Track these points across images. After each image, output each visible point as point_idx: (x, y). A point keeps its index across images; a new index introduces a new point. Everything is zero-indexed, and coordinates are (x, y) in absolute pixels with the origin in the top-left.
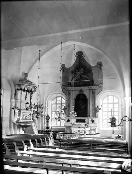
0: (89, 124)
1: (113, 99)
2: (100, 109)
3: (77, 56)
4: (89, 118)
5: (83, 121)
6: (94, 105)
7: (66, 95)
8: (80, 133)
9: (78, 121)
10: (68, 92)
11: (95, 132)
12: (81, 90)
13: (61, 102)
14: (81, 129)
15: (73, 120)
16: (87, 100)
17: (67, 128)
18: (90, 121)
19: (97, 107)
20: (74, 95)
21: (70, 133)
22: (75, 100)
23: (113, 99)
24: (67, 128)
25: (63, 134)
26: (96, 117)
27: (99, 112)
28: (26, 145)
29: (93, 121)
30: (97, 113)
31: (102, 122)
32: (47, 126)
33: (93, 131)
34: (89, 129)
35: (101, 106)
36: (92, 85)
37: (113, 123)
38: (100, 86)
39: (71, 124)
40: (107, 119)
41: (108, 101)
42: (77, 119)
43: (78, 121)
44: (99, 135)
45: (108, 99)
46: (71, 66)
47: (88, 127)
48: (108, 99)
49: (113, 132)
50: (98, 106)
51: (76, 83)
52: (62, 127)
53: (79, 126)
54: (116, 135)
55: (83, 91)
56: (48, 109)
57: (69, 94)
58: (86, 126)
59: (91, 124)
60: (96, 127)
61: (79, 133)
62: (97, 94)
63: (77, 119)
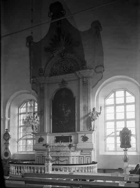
0: (78, 144)
1: (125, 97)
2: (100, 113)
3: (52, 14)
4: (77, 134)
5: (67, 139)
6: (86, 108)
7: (37, 92)
8: (60, 163)
9: (58, 140)
10: (41, 88)
11: (89, 160)
12: (63, 82)
13: (115, 116)
14: (61, 154)
15: (49, 139)
16: (75, 98)
17: (39, 153)
18: (80, 139)
19: (92, 110)
20: (51, 91)
21: (86, 163)
22: (53, 101)
23: (125, 97)
24: (39, 153)
25: (32, 166)
26: (90, 130)
27: (96, 121)
28: (52, 187)
29: (85, 139)
30: (93, 123)
31: (105, 140)
32: (6, 151)
33: (87, 158)
34: (78, 153)
35: (101, 107)
36: (83, 69)
37: (125, 144)
38: (98, 70)
39: (44, 145)
40: (113, 134)
41: (115, 101)
42: (56, 137)
43: (58, 140)
44: (96, 165)
45: (115, 97)
46: (43, 37)
47: (76, 150)
48: (115, 97)
49: (126, 160)
50: (94, 109)
51: (53, 71)
52: (20, 153)
53: (58, 149)
54: (131, 164)
55: (67, 83)
56: (11, 122)
57: (42, 90)
58: (72, 149)
59: (81, 145)
60: (92, 149)
61: (57, 163)
62: (93, 88)
63: (56, 137)
